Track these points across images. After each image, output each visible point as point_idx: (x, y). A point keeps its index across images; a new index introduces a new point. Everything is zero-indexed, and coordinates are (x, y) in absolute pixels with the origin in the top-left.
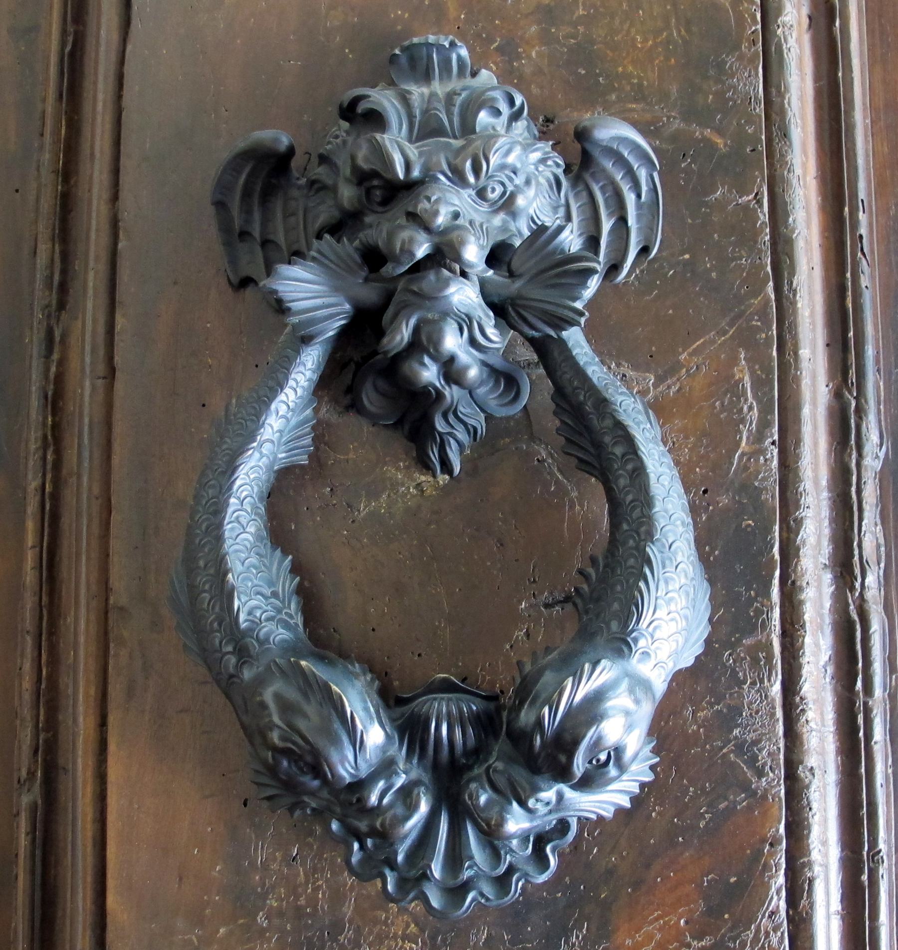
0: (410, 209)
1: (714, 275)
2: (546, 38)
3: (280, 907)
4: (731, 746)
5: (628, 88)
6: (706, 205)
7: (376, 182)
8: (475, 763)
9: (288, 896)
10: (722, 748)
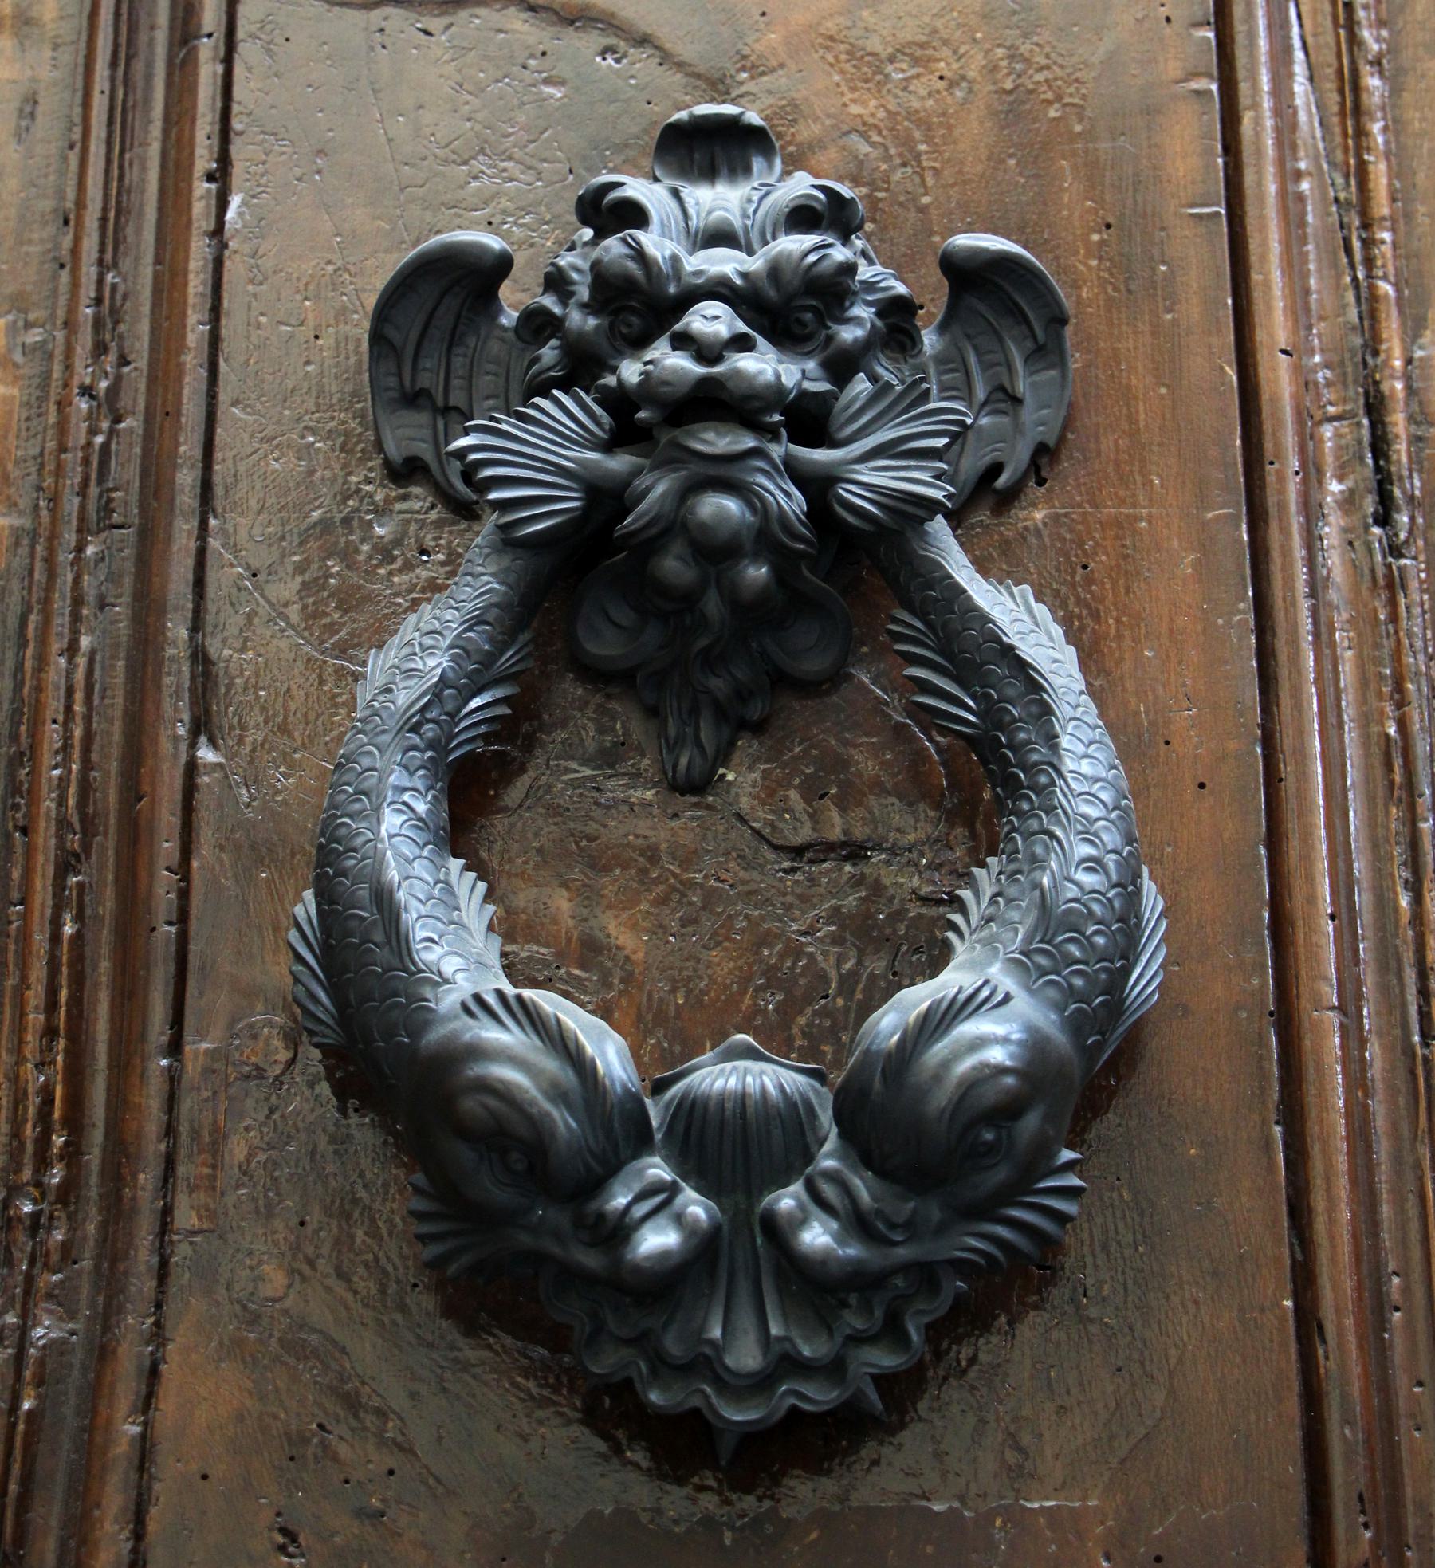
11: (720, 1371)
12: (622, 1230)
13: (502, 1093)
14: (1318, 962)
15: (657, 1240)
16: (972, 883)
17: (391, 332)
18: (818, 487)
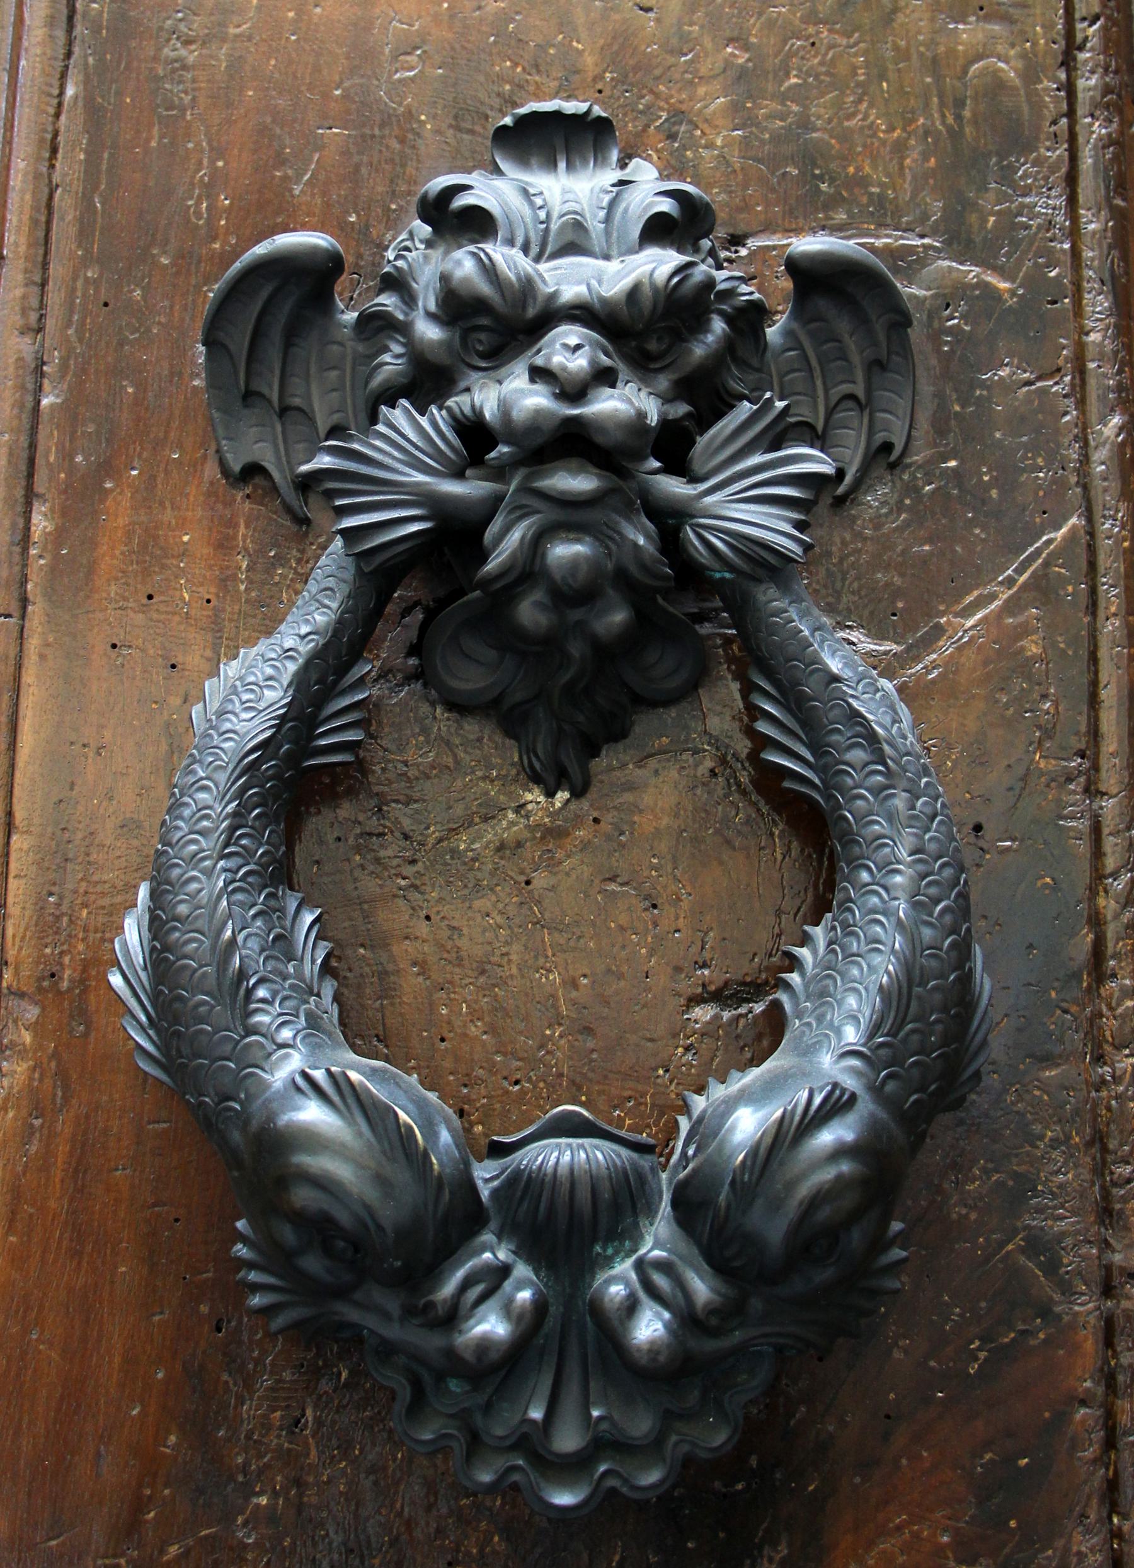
0: (539, 361)
1: (994, 493)
2: (741, 116)
3: (272, 1507)
4: (1019, 1240)
5: (865, 200)
6: (983, 385)
7: (485, 321)
8: (616, 1253)
9: (286, 1490)
10: (1002, 1244)
11: (550, 1457)
12: (452, 1317)
13: (322, 1183)
14: (768, 1098)
15: (491, 1325)
16: (805, 940)
17: (221, 335)
18: (669, 521)
